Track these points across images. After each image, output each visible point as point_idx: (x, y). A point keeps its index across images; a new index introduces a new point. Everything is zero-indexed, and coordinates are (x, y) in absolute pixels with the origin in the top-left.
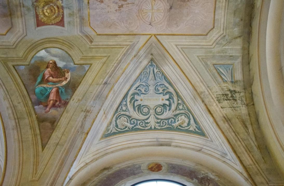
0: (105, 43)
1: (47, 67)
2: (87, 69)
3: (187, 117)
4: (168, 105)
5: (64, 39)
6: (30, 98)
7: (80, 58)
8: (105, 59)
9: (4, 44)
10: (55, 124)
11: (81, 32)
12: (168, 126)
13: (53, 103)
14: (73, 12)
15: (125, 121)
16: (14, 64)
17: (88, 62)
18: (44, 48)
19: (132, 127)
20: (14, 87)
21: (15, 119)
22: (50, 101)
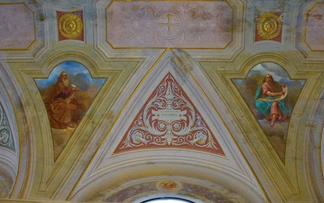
0: (319, 59)
1: (264, 82)
2: (303, 84)
3: (205, 133)
5: (280, 54)
6: (252, 112)
7: (295, 73)
8: (319, 74)
9: (222, 57)
10: (285, 138)
11: (296, 47)
12: (186, 143)
13: (275, 117)
14: (291, 28)
15: (140, 137)
16: (231, 78)
17: (303, 77)
18: (261, 63)
19: (148, 143)
20: (234, 101)
21: (243, 133)
22: (272, 115)
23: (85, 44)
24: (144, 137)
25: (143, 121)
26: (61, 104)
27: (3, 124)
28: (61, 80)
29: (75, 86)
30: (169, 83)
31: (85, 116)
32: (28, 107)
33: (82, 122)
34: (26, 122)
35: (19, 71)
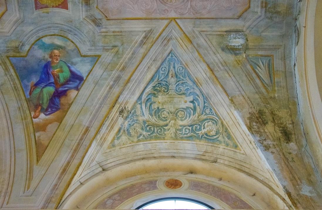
4: (193, 108)
19: (148, 135)
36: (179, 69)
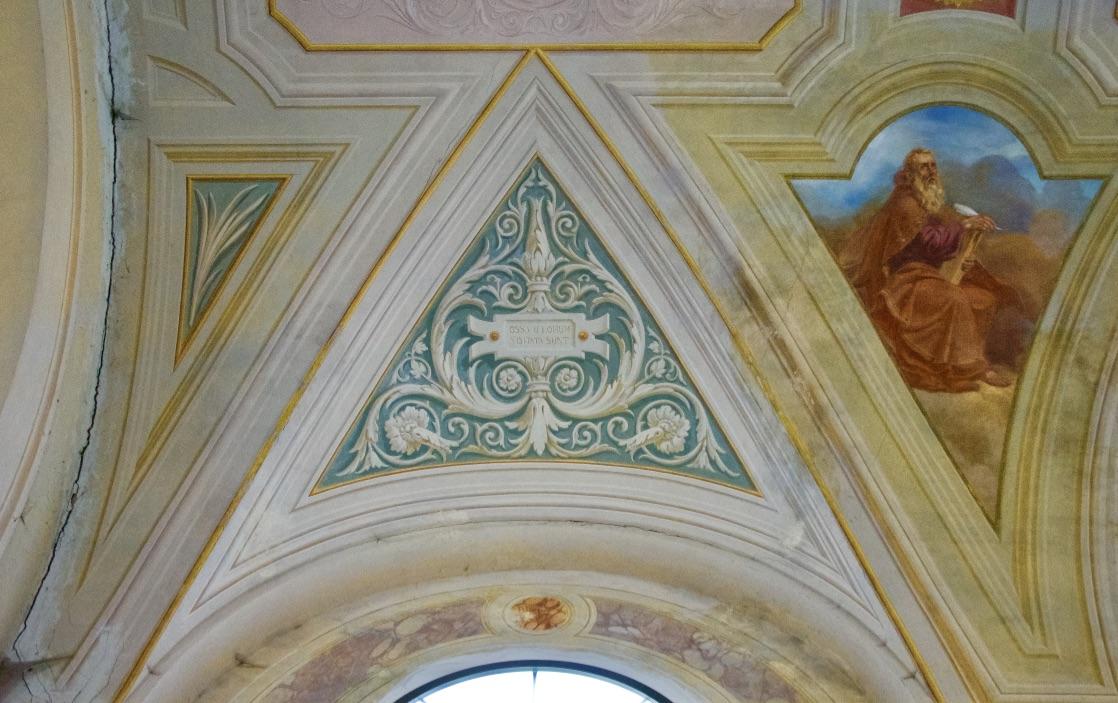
19: (452, 448)
23: (1019, 31)
24: (437, 424)
25: (431, 362)
26: (922, 287)
27: (649, 372)
28: (910, 187)
29: (970, 211)
30: (538, 204)
31: (1038, 338)
32: (780, 302)
33: (1035, 363)
34: (794, 367)
35: (716, 142)
36: (563, 225)
